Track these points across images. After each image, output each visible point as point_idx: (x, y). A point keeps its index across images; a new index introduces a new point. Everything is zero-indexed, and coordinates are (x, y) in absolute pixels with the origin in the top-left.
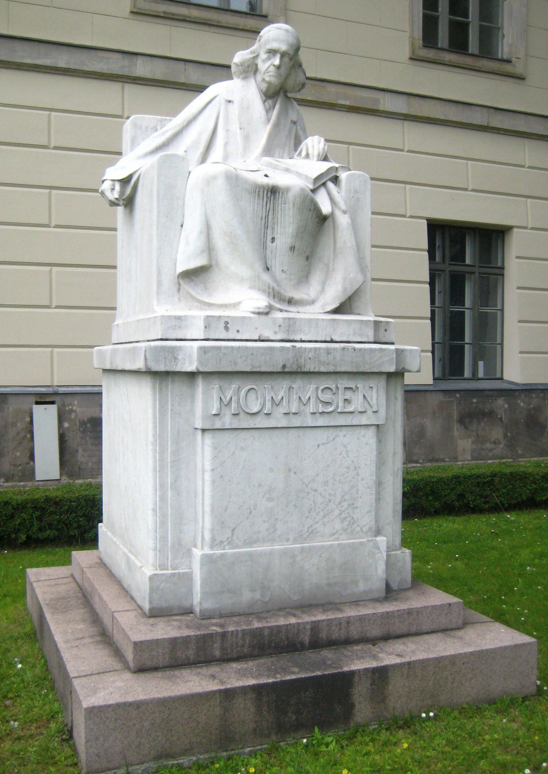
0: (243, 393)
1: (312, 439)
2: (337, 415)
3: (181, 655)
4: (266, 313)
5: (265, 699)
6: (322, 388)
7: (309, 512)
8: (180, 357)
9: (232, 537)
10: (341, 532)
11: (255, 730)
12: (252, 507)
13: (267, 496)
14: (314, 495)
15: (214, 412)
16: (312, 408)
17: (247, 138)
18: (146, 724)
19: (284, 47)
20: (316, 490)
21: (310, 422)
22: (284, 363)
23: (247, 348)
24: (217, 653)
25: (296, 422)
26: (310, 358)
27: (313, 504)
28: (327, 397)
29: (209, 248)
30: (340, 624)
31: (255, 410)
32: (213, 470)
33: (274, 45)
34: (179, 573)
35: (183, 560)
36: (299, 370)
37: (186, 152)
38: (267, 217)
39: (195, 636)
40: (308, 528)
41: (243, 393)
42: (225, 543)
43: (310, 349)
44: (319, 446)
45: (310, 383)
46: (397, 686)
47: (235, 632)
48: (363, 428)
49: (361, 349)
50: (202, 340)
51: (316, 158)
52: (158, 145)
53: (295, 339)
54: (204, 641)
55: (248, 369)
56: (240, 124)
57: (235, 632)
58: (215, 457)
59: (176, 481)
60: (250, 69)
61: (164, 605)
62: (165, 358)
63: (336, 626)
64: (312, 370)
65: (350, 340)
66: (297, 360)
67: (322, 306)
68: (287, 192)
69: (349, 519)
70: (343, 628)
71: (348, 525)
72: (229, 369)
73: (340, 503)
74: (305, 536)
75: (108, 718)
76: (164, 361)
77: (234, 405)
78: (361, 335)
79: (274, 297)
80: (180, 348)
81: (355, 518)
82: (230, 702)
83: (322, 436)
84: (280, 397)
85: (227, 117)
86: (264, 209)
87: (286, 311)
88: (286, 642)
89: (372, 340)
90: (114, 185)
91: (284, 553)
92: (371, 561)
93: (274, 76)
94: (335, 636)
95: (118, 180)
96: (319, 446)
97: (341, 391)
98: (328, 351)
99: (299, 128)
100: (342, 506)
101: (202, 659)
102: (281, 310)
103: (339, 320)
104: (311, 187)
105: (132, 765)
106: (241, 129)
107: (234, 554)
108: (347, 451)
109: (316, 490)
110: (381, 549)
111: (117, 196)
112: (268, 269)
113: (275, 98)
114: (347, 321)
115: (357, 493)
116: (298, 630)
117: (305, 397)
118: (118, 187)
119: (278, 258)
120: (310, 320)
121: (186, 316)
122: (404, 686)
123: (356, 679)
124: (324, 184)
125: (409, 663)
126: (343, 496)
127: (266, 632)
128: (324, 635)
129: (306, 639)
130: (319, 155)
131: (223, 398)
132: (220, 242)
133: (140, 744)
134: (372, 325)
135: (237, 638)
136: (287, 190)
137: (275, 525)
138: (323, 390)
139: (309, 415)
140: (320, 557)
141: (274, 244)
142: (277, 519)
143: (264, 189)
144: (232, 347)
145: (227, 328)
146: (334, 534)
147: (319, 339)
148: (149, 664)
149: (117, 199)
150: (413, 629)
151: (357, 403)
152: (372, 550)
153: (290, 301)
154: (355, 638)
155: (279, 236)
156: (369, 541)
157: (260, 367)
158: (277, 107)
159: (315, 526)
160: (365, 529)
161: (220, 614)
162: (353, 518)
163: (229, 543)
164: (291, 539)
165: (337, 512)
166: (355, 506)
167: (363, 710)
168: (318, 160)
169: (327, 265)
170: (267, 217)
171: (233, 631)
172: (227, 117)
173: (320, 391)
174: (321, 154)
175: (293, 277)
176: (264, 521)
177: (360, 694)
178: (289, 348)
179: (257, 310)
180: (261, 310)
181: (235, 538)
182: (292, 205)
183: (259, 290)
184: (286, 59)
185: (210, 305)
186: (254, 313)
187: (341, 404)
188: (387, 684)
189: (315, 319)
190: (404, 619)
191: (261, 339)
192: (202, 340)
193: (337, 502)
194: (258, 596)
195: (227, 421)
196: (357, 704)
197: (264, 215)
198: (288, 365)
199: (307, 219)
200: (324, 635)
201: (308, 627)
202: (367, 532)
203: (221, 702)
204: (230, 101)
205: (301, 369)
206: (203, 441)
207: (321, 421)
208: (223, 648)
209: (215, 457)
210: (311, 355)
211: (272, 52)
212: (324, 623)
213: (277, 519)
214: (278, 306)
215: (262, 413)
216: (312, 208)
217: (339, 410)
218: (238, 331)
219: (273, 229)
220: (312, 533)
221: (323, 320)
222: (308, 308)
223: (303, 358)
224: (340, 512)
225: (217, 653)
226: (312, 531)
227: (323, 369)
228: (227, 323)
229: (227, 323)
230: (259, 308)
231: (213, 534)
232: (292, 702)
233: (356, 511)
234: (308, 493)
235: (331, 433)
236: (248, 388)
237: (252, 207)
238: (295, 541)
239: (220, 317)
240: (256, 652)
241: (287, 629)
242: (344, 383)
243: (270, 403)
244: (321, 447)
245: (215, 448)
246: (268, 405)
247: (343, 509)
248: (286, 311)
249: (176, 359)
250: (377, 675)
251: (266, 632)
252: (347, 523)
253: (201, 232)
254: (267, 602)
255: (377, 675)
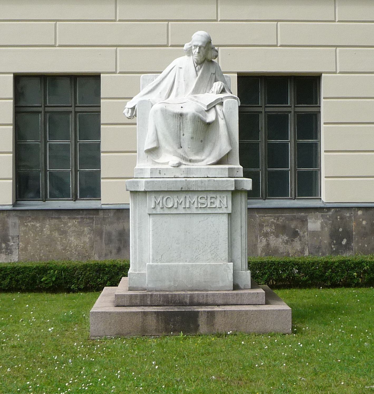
0: (165, 199)
1: (195, 220)
2: (208, 209)
3: (134, 301)
4: (179, 165)
5: (160, 317)
6: (200, 197)
7: (196, 250)
8: (139, 185)
9: (161, 258)
10: (211, 259)
11: (156, 329)
12: (170, 246)
13: (177, 242)
14: (198, 243)
15: (152, 207)
16: (195, 205)
17: (187, 85)
18: (113, 321)
19: (200, 44)
20: (199, 241)
21: (195, 211)
22: (182, 187)
23: (165, 181)
24: (149, 302)
25: (189, 212)
26: (193, 185)
27: (197, 246)
28: (203, 201)
29: (157, 140)
30: (203, 296)
31: (170, 206)
32: (153, 230)
33: (196, 43)
34: (141, 273)
35: (143, 268)
36: (188, 190)
37: (160, 93)
38: (180, 125)
39: (139, 294)
40: (196, 257)
41: (165, 199)
42: (158, 261)
43: (193, 181)
44: (200, 221)
45: (195, 195)
46: (219, 320)
47: (156, 295)
48: (221, 214)
49: (217, 181)
50: (149, 178)
51: (215, 93)
52: (149, 90)
53: (191, 177)
54: (143, 297)
55: (166, 190)
56: (184, 79)
57: (156, 295)
58: (153, 225)
59: (140, 235)
60: (189, 52)
61: (135, 286)
62: (134, 186)
63: (201, 296)
64: (194, 190)
65: (216, 177)
66: (188, 186)
67: (206, 162)
68: (187, 115)
69: (215, 254)
70: (205, 298)
71: (214, 256)
72: (158, 190)
73: (210, 247)
74: (194, 260)
75: (98, 317)
76: (133, 187)
77: (161, 204)
78: (221, 174)
79: (183, 160)
80: (139, 181)
81: (218, 254)
82: (146, 316)
83: (201, 218)
84: (181, 201)
85: (179, 75)
86: (178, 123)
87: (187, 165)
88: (179, 301)
89: (228, 176)
90: (129, 110)
91: (184, 266)
92: (225, 273)
93: (197, 56)
94: (201, 301)
95: (130, 108)
96: (200, 221)
97: (209, 199)
98: (202, 182)
99: (217, 75)
100: (212, 248)
101: (143, 304)
102: (185, 165)
103: (211, 168)
104: (206, 109)
105: (107, 336)
106: (184, 81)
107: (161, 265)
108: (213, 225)
109: (199, 241)
110: (230, 268)
111: (130, 115)
112: (179, 82)
113: (202, 64)
114: (215, 168)
115: (219, 243)
116: (184, 296)
117: (192, 201)
118: (130, 110)
119: (186, 143)
120: (197, 169)
121: (144, 168)
122: (222, 320)
123: (200, 314)
124: (214, 107)
125: (225, 311)
126: (212, 244)
127: (170, 296)
128: (195, 300)
129: (188, 301)
130: (217, 91)
131: (156, 201)
132: (161, 137)
133: (110, 328)
134: (227, 170)
135: (157, 297)
136: (187, 114)
137: (180, 255)
138: (200, 198)
139: (194, 208)
140: (201, 269)
141: (184, 136)
142: (181, 252)
143: (177, 114)
144: (159, 181)
145: (160, 173)
146: (208, 260)
147: (201, 177)
148: (121, 304)
149: (129, 116)
150: (239, 303)
151: (217, 204)
152: (226, 268)
153: (190, 161)
154: (211, 303)
155: (186, 133)
156: (224, 264)
157: (171, 188)
158: (202, 68)
159: (198, 256)
160: (223, 259)
161: (156, 290)
162: (217, 254)
163: (160, 261)
164: (188, 261)
165: (209, 251)
166: (218, 248)
167: (203, 328)
168: (217, 94)
169: (214, 144)
170: (180, 125)
171: (155, 294)
172: (179, 75)
173: (199, 199)
174: (218, 91)
175: (194, 150)
176: (175, 253)
177: (202, 321)
178: (184, 181)
179: (173, 165)
180: (174, 165)
181: (162, 259)
182: (189, 120)
183: (177, 156)
184: (202, 49)
185: (159, 163)
186: (172, 166)
187: (209, 204)
188: (214, 318)
189: (199, 168)
190: (234, 297)
191: (175, 177)
192: (149, 178)
193: (209, 246)
194: (172, 284)
195: (159, 211)
196: (200, 325)
197: (179, 125)
198: (183, 188)
199: (198, 125)
200: (196, 300)
201: (189, 296)
202: (224, 260)
203: (142, 316)
204: (181, 68)
205: (189, 189)
206: (149, 219)
207: (200, 212)
208: (151, 301)
209: (154, 225)
210: (194, 183)
211: (196, 46)
212: (195, 295)
213: (181, 252)
214: (184, 163)
215: (173, 208)
216: (200, 120)
217: (208, 207)
218: (165, 174)
219: (183, 130)
220: (197, 259)
221: (203, 168)
222: (200, 163)
223: (190, 185)
224: (210, 251)
225: (149, 302)
226: (197, 258)
227: (199, 189)
228: (160, 171)
229: (160, 171)
230: (174, 164)
231: (153, 257)
232: (172, 320)
233: (218, 250)
234: (195, 242)
235: (206, 217)
236: (167, 197)
237: (173, 122)
238: (190, 262)
239: (157, 168)
240: (165, 304)
241: (179, 296)
242: (210, 196)
243: (177, 203)
244: (201, 222)
245: (153, 221)
246: (176, 204)
247: (212, 249)
248: (187, 165)
249: (138, 186)
250: (209, 314)
251: (170, 296)
252: (214, 256)
253: (153, 133)
254: (176, 287)
255: (209, 314)
